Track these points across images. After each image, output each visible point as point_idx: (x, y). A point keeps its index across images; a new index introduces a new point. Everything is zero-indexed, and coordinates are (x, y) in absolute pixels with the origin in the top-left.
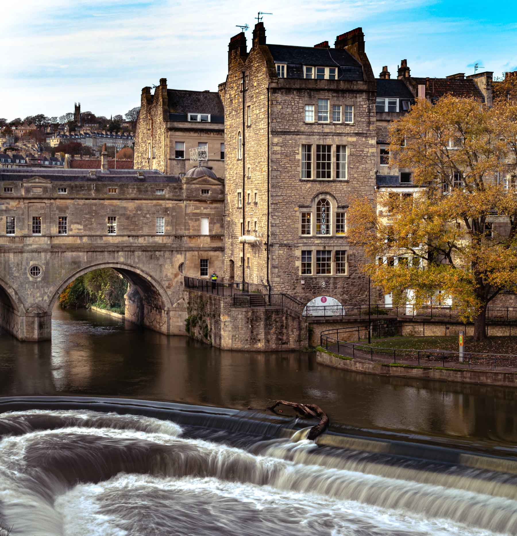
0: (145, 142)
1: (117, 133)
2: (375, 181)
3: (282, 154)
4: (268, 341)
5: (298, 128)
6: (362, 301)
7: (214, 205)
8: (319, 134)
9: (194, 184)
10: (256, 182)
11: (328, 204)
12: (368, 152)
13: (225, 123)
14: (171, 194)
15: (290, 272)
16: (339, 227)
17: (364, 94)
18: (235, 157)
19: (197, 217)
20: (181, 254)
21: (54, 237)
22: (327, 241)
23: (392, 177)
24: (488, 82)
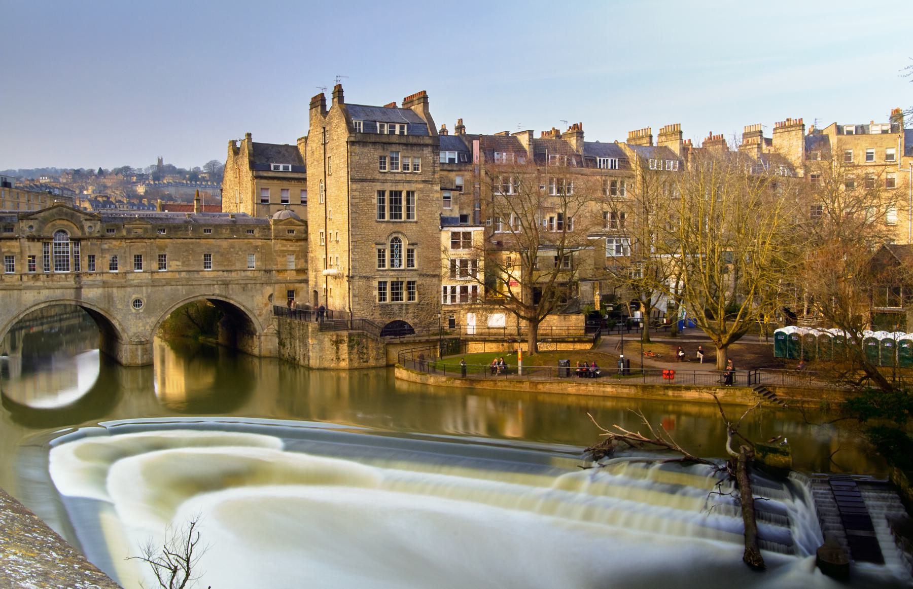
0: (233, 188)
1: (196, 182)
2: (439, 222)
3: (360, 198)
4: (351, 360)
5: (374, 176)
6: (430, 323)
7: (299, 243)
8: (392, 181)
9: (281, 225)
10: (337, 223)
11: (400, 241)
12: (433, 197)
13: (307, 172)
14: (261, 234)
15: (368, 300)
16: (410, 262)
17: (430, 147)
18: (318, 201)
19: (284, 253)
20: (270, 286)
21: (154, 272)
22: (400, 273)
23: (453, 218)
24: (530, 139)
